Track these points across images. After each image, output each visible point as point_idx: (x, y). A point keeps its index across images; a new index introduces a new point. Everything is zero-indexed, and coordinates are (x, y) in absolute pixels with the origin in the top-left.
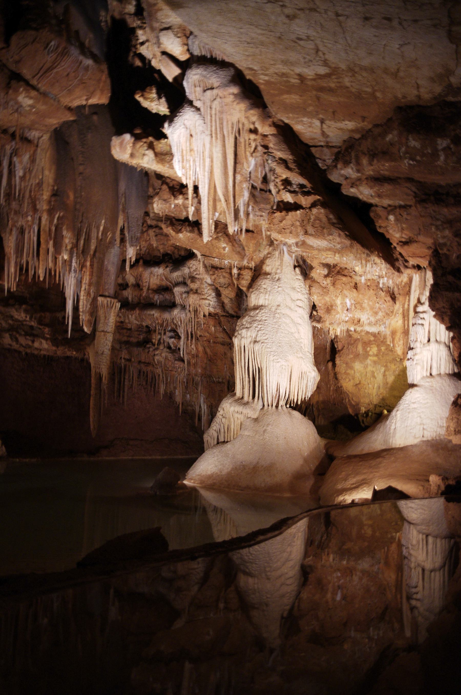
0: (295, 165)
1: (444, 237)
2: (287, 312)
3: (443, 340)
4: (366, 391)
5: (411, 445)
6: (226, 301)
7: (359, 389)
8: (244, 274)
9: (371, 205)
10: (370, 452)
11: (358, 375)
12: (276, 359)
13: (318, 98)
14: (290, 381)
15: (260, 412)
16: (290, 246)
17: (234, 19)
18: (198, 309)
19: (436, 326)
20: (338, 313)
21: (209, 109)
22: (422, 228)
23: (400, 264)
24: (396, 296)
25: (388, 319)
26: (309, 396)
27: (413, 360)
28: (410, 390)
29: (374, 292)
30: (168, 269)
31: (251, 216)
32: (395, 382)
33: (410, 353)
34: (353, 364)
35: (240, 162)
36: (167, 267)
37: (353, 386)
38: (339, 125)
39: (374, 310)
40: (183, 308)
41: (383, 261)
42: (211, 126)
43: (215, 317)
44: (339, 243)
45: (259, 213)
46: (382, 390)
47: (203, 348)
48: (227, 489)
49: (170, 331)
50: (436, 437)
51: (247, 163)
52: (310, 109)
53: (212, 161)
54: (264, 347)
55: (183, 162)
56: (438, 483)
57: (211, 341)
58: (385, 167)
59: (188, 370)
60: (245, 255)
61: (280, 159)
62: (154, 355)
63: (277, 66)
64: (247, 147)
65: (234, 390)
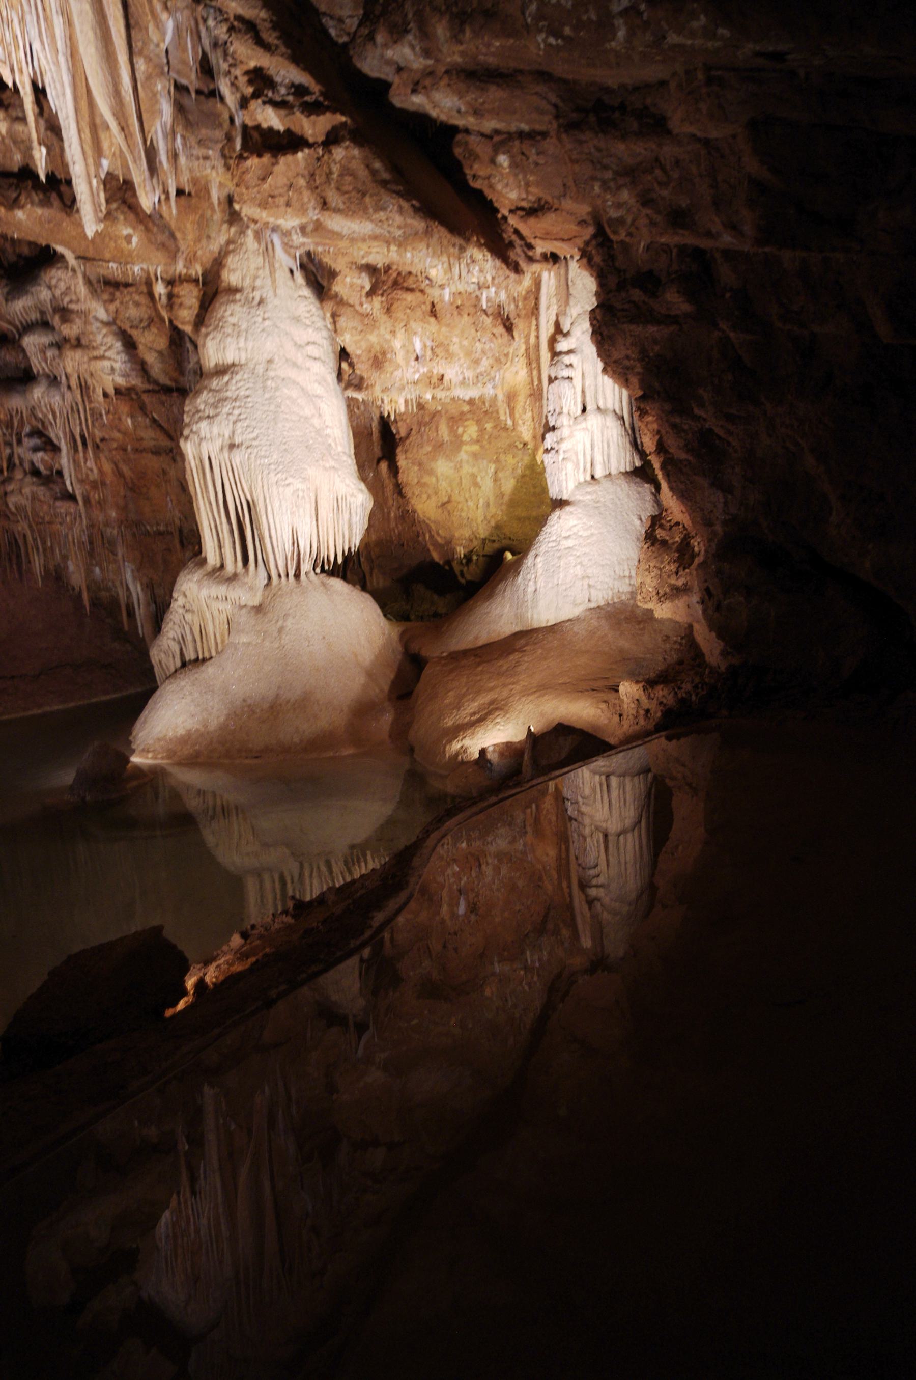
0: (275, 34)
2: (292, 373)
3: (610, 406)
4: (464, 514)
6: (151, 358)
7: (449, 512)
8: (182, 293)
10: (492, 640)
11: (444, 484)
14: (317, 520)
15: (264, 590)
16: (286, 234)
18: (89, 381)
19: (596, 378)
20: (398, 366)
22: (570, 183)
23: (516, 255)
25: (499, 370)
27: (557, 451)
28: (557, 513)
29: (471, 320)
31: (182, 160)
32: (516, 490)
33: (550, 438)
34: (433, 465)
37: (437, 507)
39: (473, 356)
40: (53, 381)
41: (488, 255)
44: (399, 227)
45: (199, 151)
46: (493, 510)
47: (113, 466)
48: (226, 761)
49: (31, 435)
50: (612, 599)
51: (157, 27)
53: (69, 23)
54: (253, 456)
56: (637, 697)
57: (129, 447)
58: (490, 49)
59: (89, 518)
61: (239, 18)
62: (6, 494)
65: (200, 552)
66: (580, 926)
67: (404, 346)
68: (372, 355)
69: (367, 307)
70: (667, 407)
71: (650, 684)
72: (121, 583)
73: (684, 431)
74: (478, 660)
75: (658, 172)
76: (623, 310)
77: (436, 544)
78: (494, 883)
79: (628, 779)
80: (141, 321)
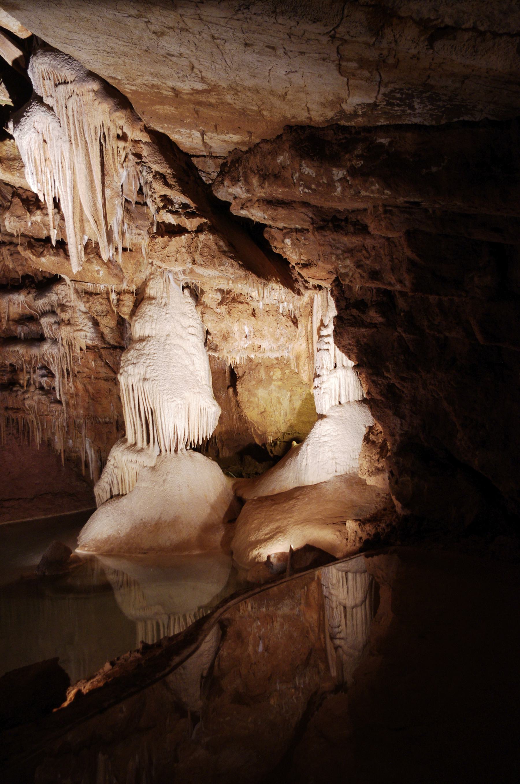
1: (346, 267)
2: (179, 342)
4: (272, 419)
5: (325, 482)
6: (106, 331)
8: (124, 299)
9: (265, 226)
10: (282, 491)
11: (262, 402)
12: (170, 398)
13: (197, 112)
14: (188, 421)
15: (157, 458)
16: (176, 274)
17: (88, 28)
20: (236, 340)
21: (64, 108)
23: (299, 285)
24: (298, 319)
26: (211, 434)
27: (320, 388)
28: (320, 422)
29: (274, 318)
30: (30, 296)
31: (127, 235)
32: (302, 407)
33: (317, 381)
34: (256, 392)
35: (108, 173)
36: (29, 293)
38: (222, 137)
40: (55, 341)
42: (69, 130)
43: (94, 349)
46: (289, 417)
47: (83, 386)
48: (127, 555)
50: (349, 471)
52: (189, 120)
54: (155, 385)
55: (37, 174)
56: (355, 529)
59: (68, 413)
60: (124, 277)
61: (157, 172)
62: (24, 399)
63: (146, 78)
64: (116, 157)
66: (330, 662)
67: (239, 330)
68: (222, 334)
69: (218, 311)
70: (370, 371)
71: (362, 522)
72: (83, 449)
73: (379, 384)
74: (273, 502)
75: (364, 252)
76: (347, 319)
77: (257, 434)
78: (279, 634)
79: (358, 575)
80: (103, 312)
